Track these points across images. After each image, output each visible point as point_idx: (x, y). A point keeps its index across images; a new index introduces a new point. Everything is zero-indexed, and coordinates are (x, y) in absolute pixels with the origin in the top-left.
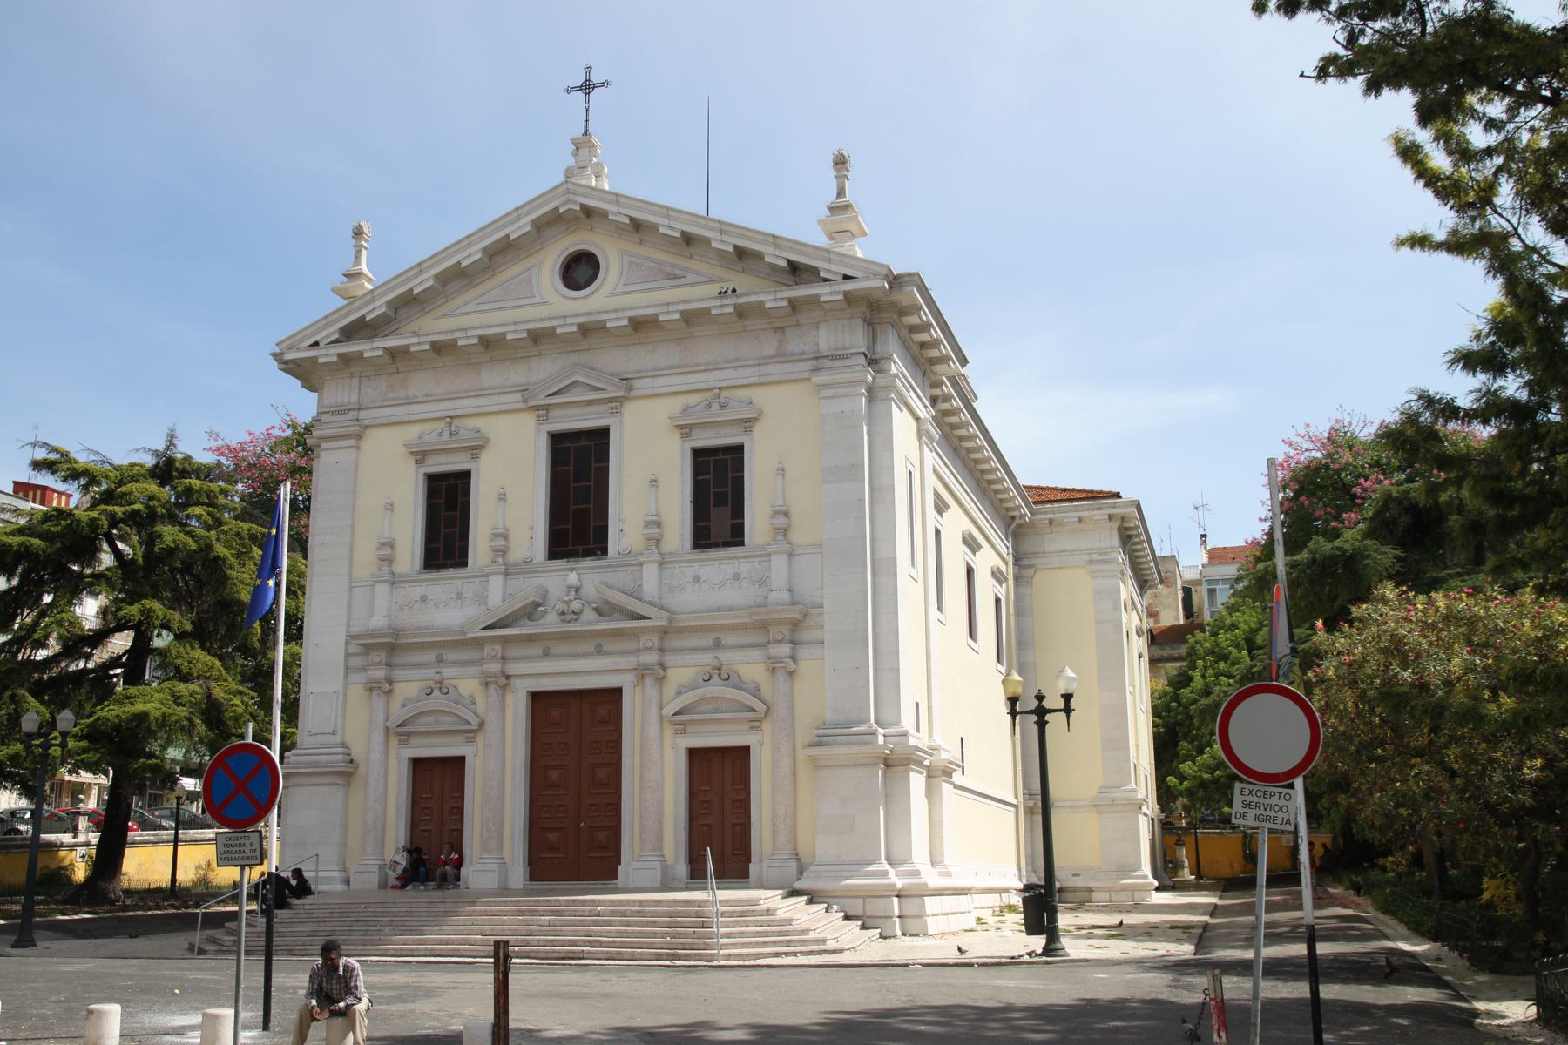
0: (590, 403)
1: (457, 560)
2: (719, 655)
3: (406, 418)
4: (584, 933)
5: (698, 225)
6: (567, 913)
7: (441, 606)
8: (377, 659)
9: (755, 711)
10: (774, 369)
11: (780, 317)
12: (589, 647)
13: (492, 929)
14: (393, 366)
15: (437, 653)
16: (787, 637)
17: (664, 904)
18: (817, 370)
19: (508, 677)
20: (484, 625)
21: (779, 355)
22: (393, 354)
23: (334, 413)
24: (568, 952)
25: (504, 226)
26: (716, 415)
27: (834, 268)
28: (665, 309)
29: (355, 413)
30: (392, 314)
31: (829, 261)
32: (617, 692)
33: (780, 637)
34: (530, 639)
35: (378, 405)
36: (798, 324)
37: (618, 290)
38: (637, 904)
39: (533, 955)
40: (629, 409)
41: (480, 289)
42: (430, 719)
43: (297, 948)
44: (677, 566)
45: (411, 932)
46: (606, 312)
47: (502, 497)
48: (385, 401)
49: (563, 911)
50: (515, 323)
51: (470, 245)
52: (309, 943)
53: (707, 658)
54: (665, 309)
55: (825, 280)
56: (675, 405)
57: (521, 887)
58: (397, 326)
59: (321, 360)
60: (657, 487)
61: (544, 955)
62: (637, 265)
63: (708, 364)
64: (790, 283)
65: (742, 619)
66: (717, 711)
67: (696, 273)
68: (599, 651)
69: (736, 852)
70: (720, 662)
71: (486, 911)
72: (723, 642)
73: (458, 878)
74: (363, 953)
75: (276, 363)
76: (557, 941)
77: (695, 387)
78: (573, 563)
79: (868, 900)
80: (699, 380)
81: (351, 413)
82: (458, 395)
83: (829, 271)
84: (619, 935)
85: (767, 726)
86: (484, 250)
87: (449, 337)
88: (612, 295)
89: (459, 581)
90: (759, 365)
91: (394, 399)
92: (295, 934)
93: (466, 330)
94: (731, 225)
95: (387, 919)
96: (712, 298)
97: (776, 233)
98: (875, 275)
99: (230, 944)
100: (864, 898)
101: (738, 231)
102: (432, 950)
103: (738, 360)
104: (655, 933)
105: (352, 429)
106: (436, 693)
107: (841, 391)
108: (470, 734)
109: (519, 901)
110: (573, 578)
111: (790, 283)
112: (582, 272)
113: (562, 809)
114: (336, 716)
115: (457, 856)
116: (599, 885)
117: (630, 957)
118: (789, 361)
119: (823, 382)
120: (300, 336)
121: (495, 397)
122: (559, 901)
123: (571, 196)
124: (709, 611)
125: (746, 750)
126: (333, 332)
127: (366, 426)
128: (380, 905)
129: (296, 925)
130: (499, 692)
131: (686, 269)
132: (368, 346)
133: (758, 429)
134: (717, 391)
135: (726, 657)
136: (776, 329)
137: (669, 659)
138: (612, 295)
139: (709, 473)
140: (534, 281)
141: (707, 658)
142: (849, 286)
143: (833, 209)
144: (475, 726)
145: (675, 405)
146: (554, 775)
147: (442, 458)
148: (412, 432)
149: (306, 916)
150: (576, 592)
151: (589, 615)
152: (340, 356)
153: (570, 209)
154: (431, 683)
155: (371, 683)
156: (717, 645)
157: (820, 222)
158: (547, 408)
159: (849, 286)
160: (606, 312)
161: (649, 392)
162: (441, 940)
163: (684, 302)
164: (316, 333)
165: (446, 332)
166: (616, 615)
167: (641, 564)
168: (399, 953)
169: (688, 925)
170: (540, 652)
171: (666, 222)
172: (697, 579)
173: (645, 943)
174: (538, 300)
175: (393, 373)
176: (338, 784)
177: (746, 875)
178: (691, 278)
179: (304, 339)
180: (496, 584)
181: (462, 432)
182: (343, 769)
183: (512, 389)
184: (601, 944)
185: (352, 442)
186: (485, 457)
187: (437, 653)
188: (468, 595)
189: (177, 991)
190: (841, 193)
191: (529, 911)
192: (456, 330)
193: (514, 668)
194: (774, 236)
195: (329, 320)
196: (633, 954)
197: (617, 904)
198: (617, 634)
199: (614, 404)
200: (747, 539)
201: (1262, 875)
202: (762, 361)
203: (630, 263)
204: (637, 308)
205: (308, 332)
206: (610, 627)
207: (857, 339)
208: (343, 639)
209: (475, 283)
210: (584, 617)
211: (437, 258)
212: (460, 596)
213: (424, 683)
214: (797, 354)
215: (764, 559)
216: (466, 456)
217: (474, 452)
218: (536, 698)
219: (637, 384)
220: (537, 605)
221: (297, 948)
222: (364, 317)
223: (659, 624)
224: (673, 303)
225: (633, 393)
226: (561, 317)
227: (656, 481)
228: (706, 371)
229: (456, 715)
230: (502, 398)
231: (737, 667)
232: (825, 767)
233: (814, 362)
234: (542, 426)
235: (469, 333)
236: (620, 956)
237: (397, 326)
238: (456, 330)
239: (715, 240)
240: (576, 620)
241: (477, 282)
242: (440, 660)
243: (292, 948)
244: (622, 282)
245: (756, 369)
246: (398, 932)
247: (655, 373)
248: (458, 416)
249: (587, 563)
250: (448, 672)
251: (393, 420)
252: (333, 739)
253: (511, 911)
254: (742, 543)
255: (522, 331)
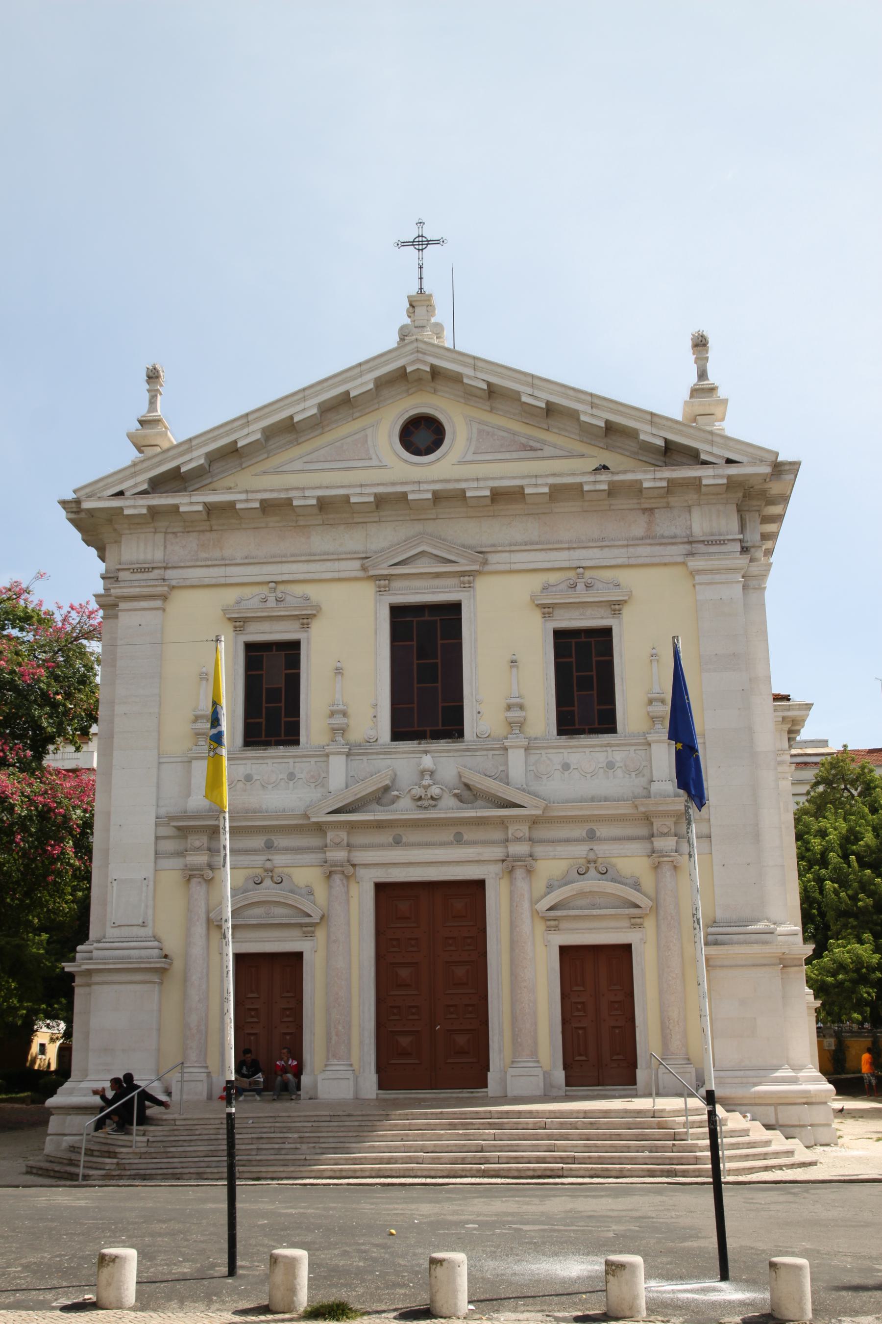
0: (438, 575)
1: (283, 738)
2: (595, 848)
3: (222, 581)
4: (545, 1148)
5: (568, 397)
6: (507, 1126)
7: (270, 787)
8: (197, 844)
9: (638, 906)
10: (644, 550)
11: (651, 498)
12: (447, 835)
13: (435, 1146)
14: (208, 523)
15: (265, 838)
16: (673, 830)
17: (613, 1115)
18: (691, 554)
19: (354, 865)
20: (330, 809)
21: (649, 537)
22: (211, 509)
23: (134, 571)
24: (545, 1169)
25: (344, 382)
26: (581, 595)
27: (716, 450)
28: (533, 481)
29: (161, 572)
30: (207, 467)
31: (712, 443)
32: (480, 885)
33: (666, 830)
34: (379, 825)
35: (188, 564)
36: (668, 507)
37: (469, 457)
38: (582, 1115)
39: (502, 1173)
40: (483, 585)
41: (305, 448)
42: (257, 911)
43: (208, 1170)
44: (543, 752)
45: (335, 1150)
46: (466, 480)
47: (339, 671)
48: (197, 560)
49: (503, 1123)
50: (361, 486)
51: (304, 399)
52: (214, 1164)
53: (581, 850)
54: (533, 481)
55: (705, 463)
56: (536, 582)
57: (374, 1097)
58: (209, 480)
59: (127, 512)
60: (517, 667)
61: (516, 1174)
62: (488, 433)
63: (571, 542)
64: (660, 463)
65: (625, 809)
66: (594, 906)
67: (554, 446)
68: (459, 840)
69: (615, 1058)
70: (596, 855)
71: (410, 1124)
72: (598, 834)
73: (298, 1088)
74: (294, 1175)
75: (64, 512)
76: (523, 1157)
77: (343, 575)
78: (424, 745)
79: (780, 1107)
80: (561, 558)
81: (156, 572)
82: (284, 559)
83: (711, 453)
84: (586, 1149)
85: (649, 924)
86: (320, 405)
87: (283, 495)
88: (460, 463)
89: (291, 760)
90: (627, 546)
91: (207, 559)
92: (189, 1154)
93: (303, 489)
94: (605, 399)
95: (296, 1135)
96: (584, 474)
97: (654, 411)
98: (762, 461)
99: (113, 1167)
100: (776, 1105)
101: (611, 406)
102: (380, 1170)
103: (603, 539)
104: (629, 1147)
105: (159, 589)
106: (268, 882)
107: (718, 578)
108: (308, 928)
109: (441, 1113)
110: (427, 761)
111: (660, 463)
112: (422, 437)
113: (414, 1010)
114: (147, 907)
115: (295, 1063)
116: (465, 1094)
117: (618, 1174)
118: (661, 544)
119: (700, 568)
120: (101, 484)
121: (329, 564)
122: (490, 1112)
123: (420, 355)
124: (582, 800)
125: (627, 948)
126: (141, 481)
127: (174, 587)
128: (271, 1120)
129: (181, 1143)
130: (345, 882)
131: (544, 442)
132: (649, 476)
133: (627, 612)
134: (272, 585)
135: (602, 849)
136: (644, 510)
137: (539, 850)
138: (460, 463)
139: (570, 656)
140: (370, 443)
141: (581, 850)
142: (733, 470)
143: (695, 392)
144: (316, 919)
145: (536, 582)
146: (404, 973)
147: (265, 626)
148: (230, 596)
149: (186, 1133)
150: (431, 776)
151: (449, 801)
152: (150, 508)
153: (418, 369)
154: (259, 871)
155: (192, 870)
156: (591, 836)
157: (130, 436)
158: (388, 577)
159: (733, 470)
160: (466, 480)
161: (507, 567)
162: (382, 1158)
163: (554, 475)
164: (122, 481)
165: (279, 491)
166: (479, 802)
167: (327, 755)
168: (338, 1174)
169: (657, 1137)
170: (391, 840)
171: (529, 390)
172: (566, 767)
173: (626, 1158)
174: (374, 462)
175: (203, 531)
176: (155, 983)
177: (633, 1081)
178: (548, 451)
179: (106, 487)
180: (338, 768)
181: (289, 598)
182: (158, 965)
183: (349, 556)
184: (574, 1160)
185: (158, 603)
186: (316, 627)
187: (265, 838)
188: (302, 776)
189: (393, 1231)
190: (702, 375)
191: (462, 1124)
192: (292, 489)
193: (360, 857)
194: (652, 414)
195: (138, 468)
196: (621, 1170)
197: (558, 1115)
198: (480, 822)
199: (467, 578)
200: (302, 739)
201: (230, 1063)
202: (631, 543)
203: (480, 432)
204: (502, 478)
205: (110, 480)
206: (479, 814)
207: (729, 524)
208: (152, 820)
209: (300, 440)
210: (442, 804)
211: (267, 410)
212: (291, 776)
213: (250, 871)
214: (668, 537)
215: (641, 747)
216: (296, 625)
217: (305, 621)
218: (381, 888)
219: (493, 558)
220: (386, 789)
221: (208, 1170)
222: (178, 468)
223: (533, 812)
224: (541, 476)
225: (488, 568)
226: (414, 482)
227: (656, 655)
228: (569, 549)
229: (296, 908)
230: (337, 565)
231: (614, 860)
232: (722, 967)
233: (687, 547)
234: (383, 597)
235: (307, 493)
236: (606, 1173)
237: (209, 480)
238: (292, 489)
239: (585, 413)
240: (435, 806)
241: (303, 439)
242: (269, 846)
243: (201, 1170)
244: (472, 449)
245: (624, 550)
246: (319, 1151)
247: (513, 548)
248: (283, 582)
249: (442, 745)
250: (279, 860)
251: (207, 581)
252: (142, 932)
253: (440, 1124)
254: (612, 730)
255: (368, 494)
